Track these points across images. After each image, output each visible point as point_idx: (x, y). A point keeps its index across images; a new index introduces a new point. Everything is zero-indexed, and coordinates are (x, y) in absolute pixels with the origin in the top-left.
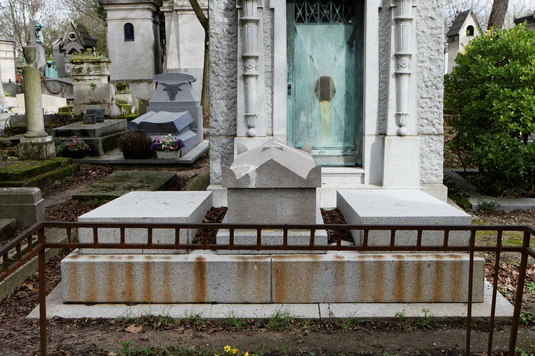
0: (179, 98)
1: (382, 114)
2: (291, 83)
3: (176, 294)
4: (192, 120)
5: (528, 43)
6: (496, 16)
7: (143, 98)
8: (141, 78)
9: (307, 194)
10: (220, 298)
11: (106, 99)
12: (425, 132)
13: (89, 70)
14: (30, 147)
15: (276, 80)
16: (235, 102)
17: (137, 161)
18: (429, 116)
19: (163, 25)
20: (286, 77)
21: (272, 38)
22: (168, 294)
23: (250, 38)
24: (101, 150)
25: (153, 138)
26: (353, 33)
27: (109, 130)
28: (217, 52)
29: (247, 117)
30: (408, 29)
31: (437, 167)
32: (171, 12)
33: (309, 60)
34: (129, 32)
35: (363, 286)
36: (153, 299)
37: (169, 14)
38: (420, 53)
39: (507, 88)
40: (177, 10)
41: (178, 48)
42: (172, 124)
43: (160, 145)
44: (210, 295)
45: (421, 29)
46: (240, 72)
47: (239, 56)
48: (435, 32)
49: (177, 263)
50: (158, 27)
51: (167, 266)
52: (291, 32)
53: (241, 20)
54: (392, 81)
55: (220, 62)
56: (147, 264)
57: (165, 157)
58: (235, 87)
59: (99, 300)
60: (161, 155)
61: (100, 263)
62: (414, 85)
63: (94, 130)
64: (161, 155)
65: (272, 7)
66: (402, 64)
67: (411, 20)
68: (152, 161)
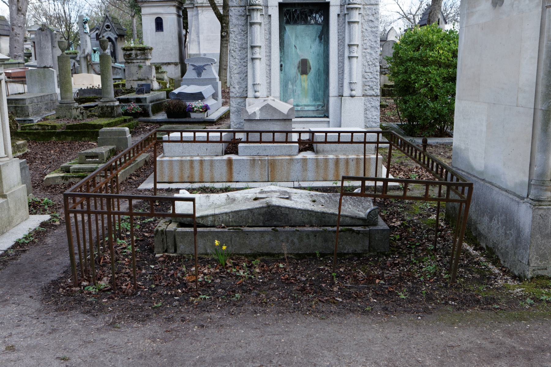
0: (204, 75)
1: (340, 82)
2: (282, 63)
3: (217, 177)
4: (214, 91)
5: (435, 37)
6: (433, 14)
7: (171, 77)
8: (169, 61)
9: (287, 123)
10: (241, 179)
11: (149, 76)
12: (368, 94)
13: (136, 55)
14: (105, 109)
15: (272, 61)
16: (246, 76)
17: (177, 120)
18: (371, 84)
19: (185, 17)
20: (279, 59)
21: (270, 34)
22: (212, 177)
23: (256, 34)
24: (151, 113)
25: (188, 103)
26: (322, 30)
27: (155, 98)
28: (235, 43)
29: (254, 85)
30: (356, 29)
31: (375, 117)
32: (193, 8)
33: (294, 48)
34: (159, 24)
35: (317, 172)
36: (204, 180)
37: (191, 10)
38: (365, 44)
39: (421, 66)
40: (197, 7)
41: (198, 37)
42: (200, 93)
43: (193, 108)
44: (235, 178)
45: (365, 28)
46: (249, 56)
47: (249, 46)
48: (374, 29)
49: (217, 160)
50: (182, 20)
51: (212, 162)
52: (282, 30)
53: (250, 23)
54: (346, 61)
55: (237, 50)
56: (201, 160)
57: (196, 117)
58: (247, 66)
59: (175, 181)
60: (193, 115)
61: (176, 161)
62: (360, 64)
63: (146, 98)
64: (193, 115)
65: (269, 14)
66: (352, 50)
67: (358, 22)
68: (187, 119)
